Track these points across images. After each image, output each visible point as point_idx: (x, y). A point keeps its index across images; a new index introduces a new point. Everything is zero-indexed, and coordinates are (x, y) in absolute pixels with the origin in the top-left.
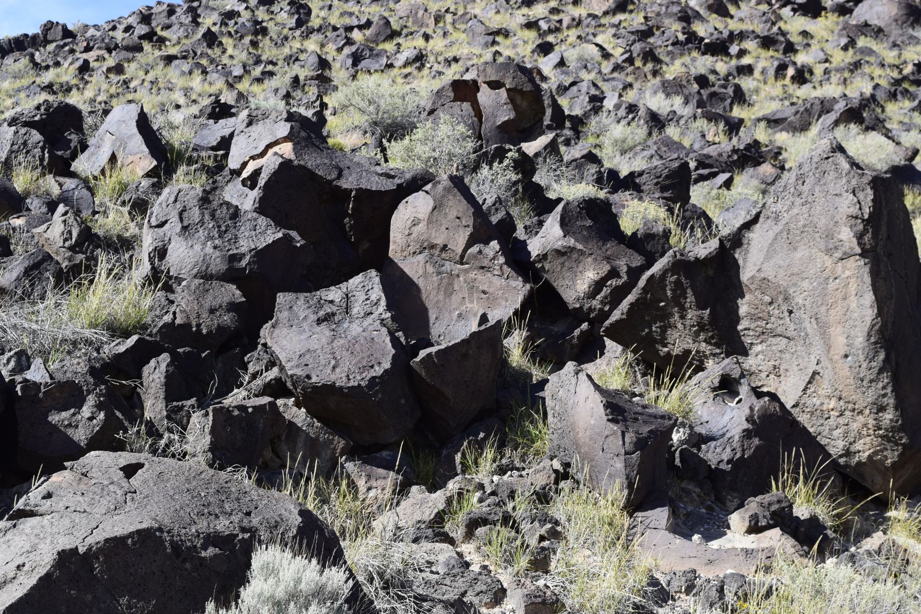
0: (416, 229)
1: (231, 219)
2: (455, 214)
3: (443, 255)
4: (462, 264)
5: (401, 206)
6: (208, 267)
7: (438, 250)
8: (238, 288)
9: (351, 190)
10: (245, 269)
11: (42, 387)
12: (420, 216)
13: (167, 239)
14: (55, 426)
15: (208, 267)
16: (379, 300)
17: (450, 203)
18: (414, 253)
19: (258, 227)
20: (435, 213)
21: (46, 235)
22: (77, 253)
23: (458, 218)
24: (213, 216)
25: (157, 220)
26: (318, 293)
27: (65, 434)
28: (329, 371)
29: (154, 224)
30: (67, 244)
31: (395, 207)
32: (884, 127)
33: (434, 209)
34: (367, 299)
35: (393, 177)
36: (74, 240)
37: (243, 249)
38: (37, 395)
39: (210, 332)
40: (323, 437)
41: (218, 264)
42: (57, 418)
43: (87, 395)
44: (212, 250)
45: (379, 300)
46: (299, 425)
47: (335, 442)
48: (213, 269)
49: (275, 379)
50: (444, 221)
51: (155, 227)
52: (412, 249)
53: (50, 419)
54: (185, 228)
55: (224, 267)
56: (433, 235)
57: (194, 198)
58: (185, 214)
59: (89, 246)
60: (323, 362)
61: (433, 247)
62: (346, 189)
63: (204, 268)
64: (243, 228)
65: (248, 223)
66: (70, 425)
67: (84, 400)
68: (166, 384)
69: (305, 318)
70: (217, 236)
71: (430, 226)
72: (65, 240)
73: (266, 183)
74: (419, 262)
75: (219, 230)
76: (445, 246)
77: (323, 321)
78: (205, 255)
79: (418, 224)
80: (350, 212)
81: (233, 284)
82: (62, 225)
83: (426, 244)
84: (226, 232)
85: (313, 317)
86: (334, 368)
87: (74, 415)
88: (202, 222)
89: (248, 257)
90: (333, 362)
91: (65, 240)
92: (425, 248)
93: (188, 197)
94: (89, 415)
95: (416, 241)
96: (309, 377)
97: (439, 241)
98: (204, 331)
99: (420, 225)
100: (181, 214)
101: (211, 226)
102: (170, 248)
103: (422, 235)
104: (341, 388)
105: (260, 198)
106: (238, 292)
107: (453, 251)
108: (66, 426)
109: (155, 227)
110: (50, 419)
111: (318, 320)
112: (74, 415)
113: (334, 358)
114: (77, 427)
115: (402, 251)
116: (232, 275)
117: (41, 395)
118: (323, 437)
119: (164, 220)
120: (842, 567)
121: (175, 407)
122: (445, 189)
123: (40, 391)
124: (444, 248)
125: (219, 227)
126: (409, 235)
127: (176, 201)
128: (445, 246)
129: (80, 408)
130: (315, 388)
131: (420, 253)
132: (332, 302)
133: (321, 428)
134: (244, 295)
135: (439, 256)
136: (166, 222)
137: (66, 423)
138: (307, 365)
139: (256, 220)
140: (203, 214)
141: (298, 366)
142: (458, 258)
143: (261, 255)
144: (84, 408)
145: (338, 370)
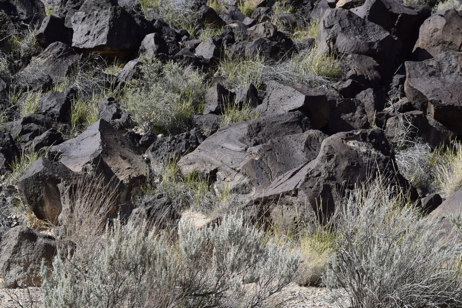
0: (436, 35)
1: (363, 25)
2: (457, 27)
3: (450, 47)
4: (459, 51)
5: (426, 22)
6: (359, 48)
7: (447, 44)
8: (374, 59)
9: (399, 14)
10: (376, 50)
11: (337, 102)
12: (438, 27)
13: (335, 34)
14: (344, 121)
15: (359, 48)
16: (456, 66)
17: (455, 21)
18: (434, 46)
19: (376, 30)
20: (447, 26)
21: (255, 32)
22: (273, 41)
23: (458, 29)
24: (354, 23)
25: (328, 25)
26: (423, 62)
27: (350, 125)
28: (449, 99)
29: (327, 27)
30: (268, 36)
31: (422, 22)
32: (32, 9)
33: (446, 24)
34: (450, 65)
35: (413, 9)
36: (272, 34)
37: (250, 46)
38: (335, 105)
39: (372, 79)
40: (443, 131)
41: (364, 48)
42: (345, 117)
43: (357, 106)
44: (360, 40)
45: (456, 66)
46: (432, 125)
47: (449, 133)
48: (362, 49)
49: (408, 103)
50: (451, 30)
51: (328, 28)
52: (432, 44)
53: (342, 117)
54: (343, 29)
55: (367, 49)
56: (445, 37)
57: (345, 14)
58: (341, 22)
59: (279, 38)
60: (445, 94)
61: (444, 42)
62: (396, 14)
63: (357, 49)
64: (369, 30)
65: (371, 28)
66: (351, 120)
67: (356, 109)
68: (375, 103)
69: (423, 73)
70: (358, 33)
71: (444, 32)
72: (267, 34)
73: (371, 8)
74: (438, 50)
75: (359, 31)
76: (451, 42)
77: (432, 75)
78: (357, 43)
79: (437, 31)
80: (396, 25)
81: (371, 57)
82: (263, 27)
83: (441, 41)
84: (362, 31)
85: (427, 74)
86: (451, 97)
87: (352, 115)
88: (350, 26)
89: (376, 44)
90: (450, 95)
91: (267, 34)
92: (440, 43)
93: (341, 14)
94: (359, 116)
95: (436, 40)
96: (440, 101)
97: (448, 39)
98: (370, 79)
99: (438, 32)
100: (340, 22)
101: (354, 28)
102: (338, 38)
103: (439, 36)
104: (457, 107)
105: (368, 16)
106: (374, 61)
107: (455, 45)
108: (350, 121)
109: (328, 28)
110: (342, 117)
111: (430, 74)
112: (352, 115)
113: (450, 92)
114: (355, 121)
115: (427, 44)
116: (370, 53)
117: (337, 105)
118: (443, 131)
119: (332, 24)
120: (406, 209)
121: (380, 114)
122: (452, 14)
123: (336, 103)
124: (451, 43)
125: (358, 29)
126: (432, 36)
127: (336, 16)
128: (451, 42)
129: (355, 112)
130: (444, 107)
131: (437, 46)
132: (432, 66)
133: (442, 126)
134: (378, 63)
135: (447, 47)
136: (333, 26)
137: (350, 119)
138: (437, 96)
139: (374, 26)
140: (350, 22)
141: (433, 96)
142: (458, 48)
143: (382, 43)
144: (356, 113)
145: (453, 98)
